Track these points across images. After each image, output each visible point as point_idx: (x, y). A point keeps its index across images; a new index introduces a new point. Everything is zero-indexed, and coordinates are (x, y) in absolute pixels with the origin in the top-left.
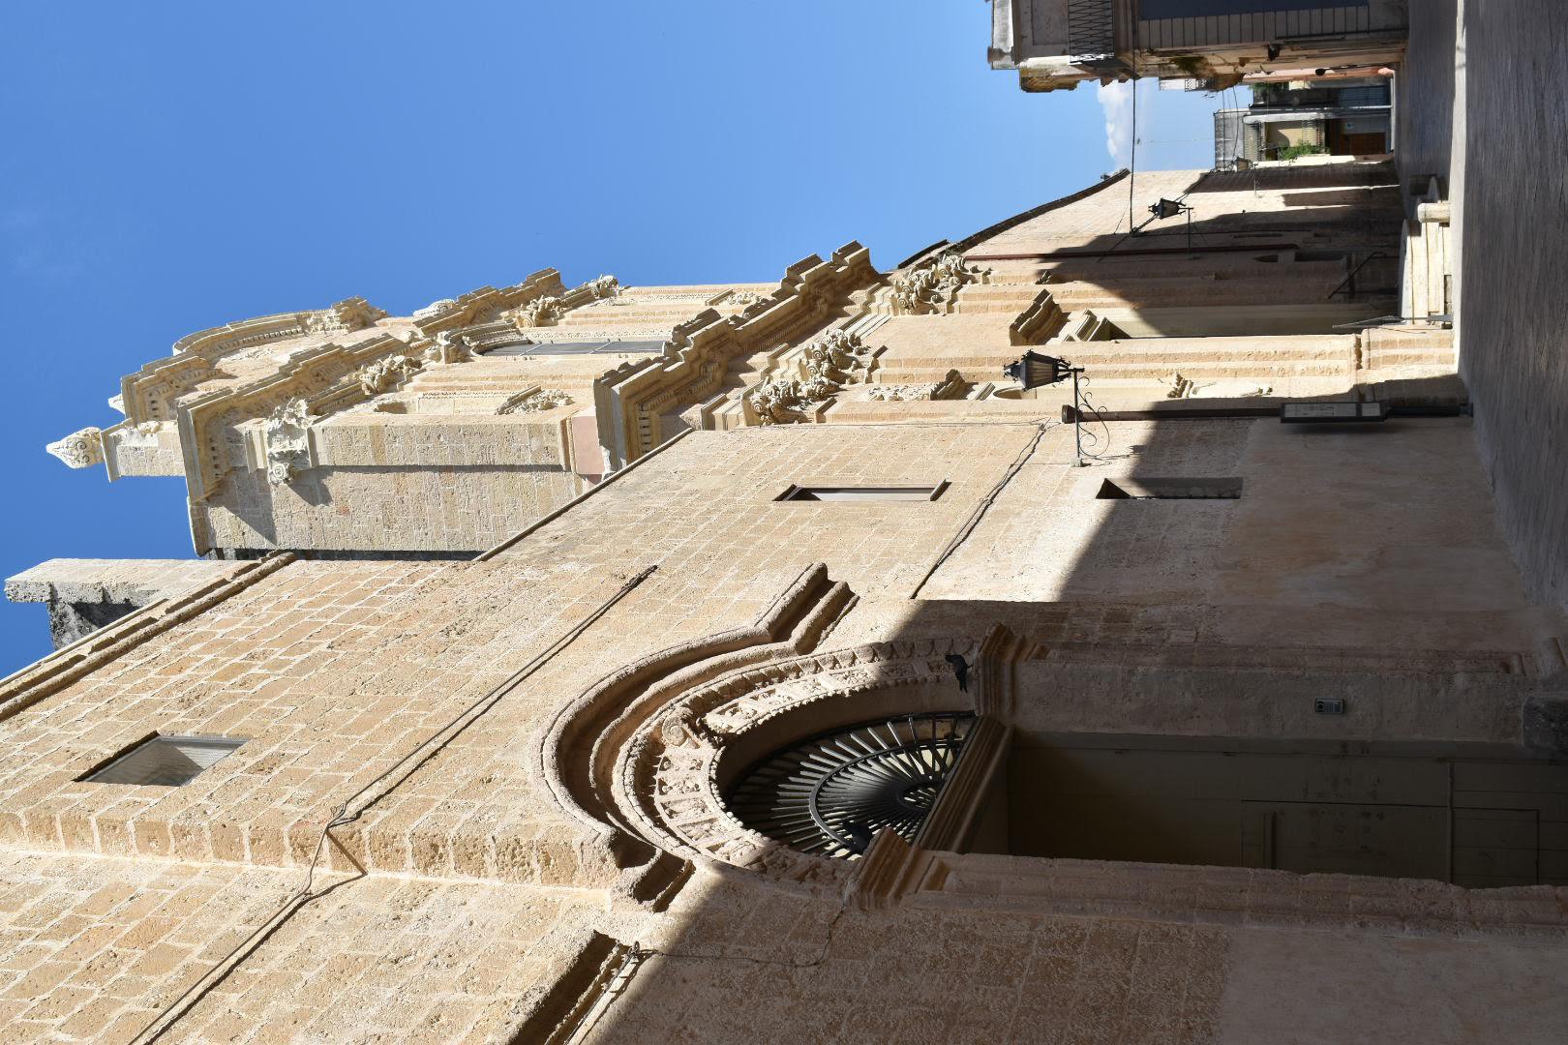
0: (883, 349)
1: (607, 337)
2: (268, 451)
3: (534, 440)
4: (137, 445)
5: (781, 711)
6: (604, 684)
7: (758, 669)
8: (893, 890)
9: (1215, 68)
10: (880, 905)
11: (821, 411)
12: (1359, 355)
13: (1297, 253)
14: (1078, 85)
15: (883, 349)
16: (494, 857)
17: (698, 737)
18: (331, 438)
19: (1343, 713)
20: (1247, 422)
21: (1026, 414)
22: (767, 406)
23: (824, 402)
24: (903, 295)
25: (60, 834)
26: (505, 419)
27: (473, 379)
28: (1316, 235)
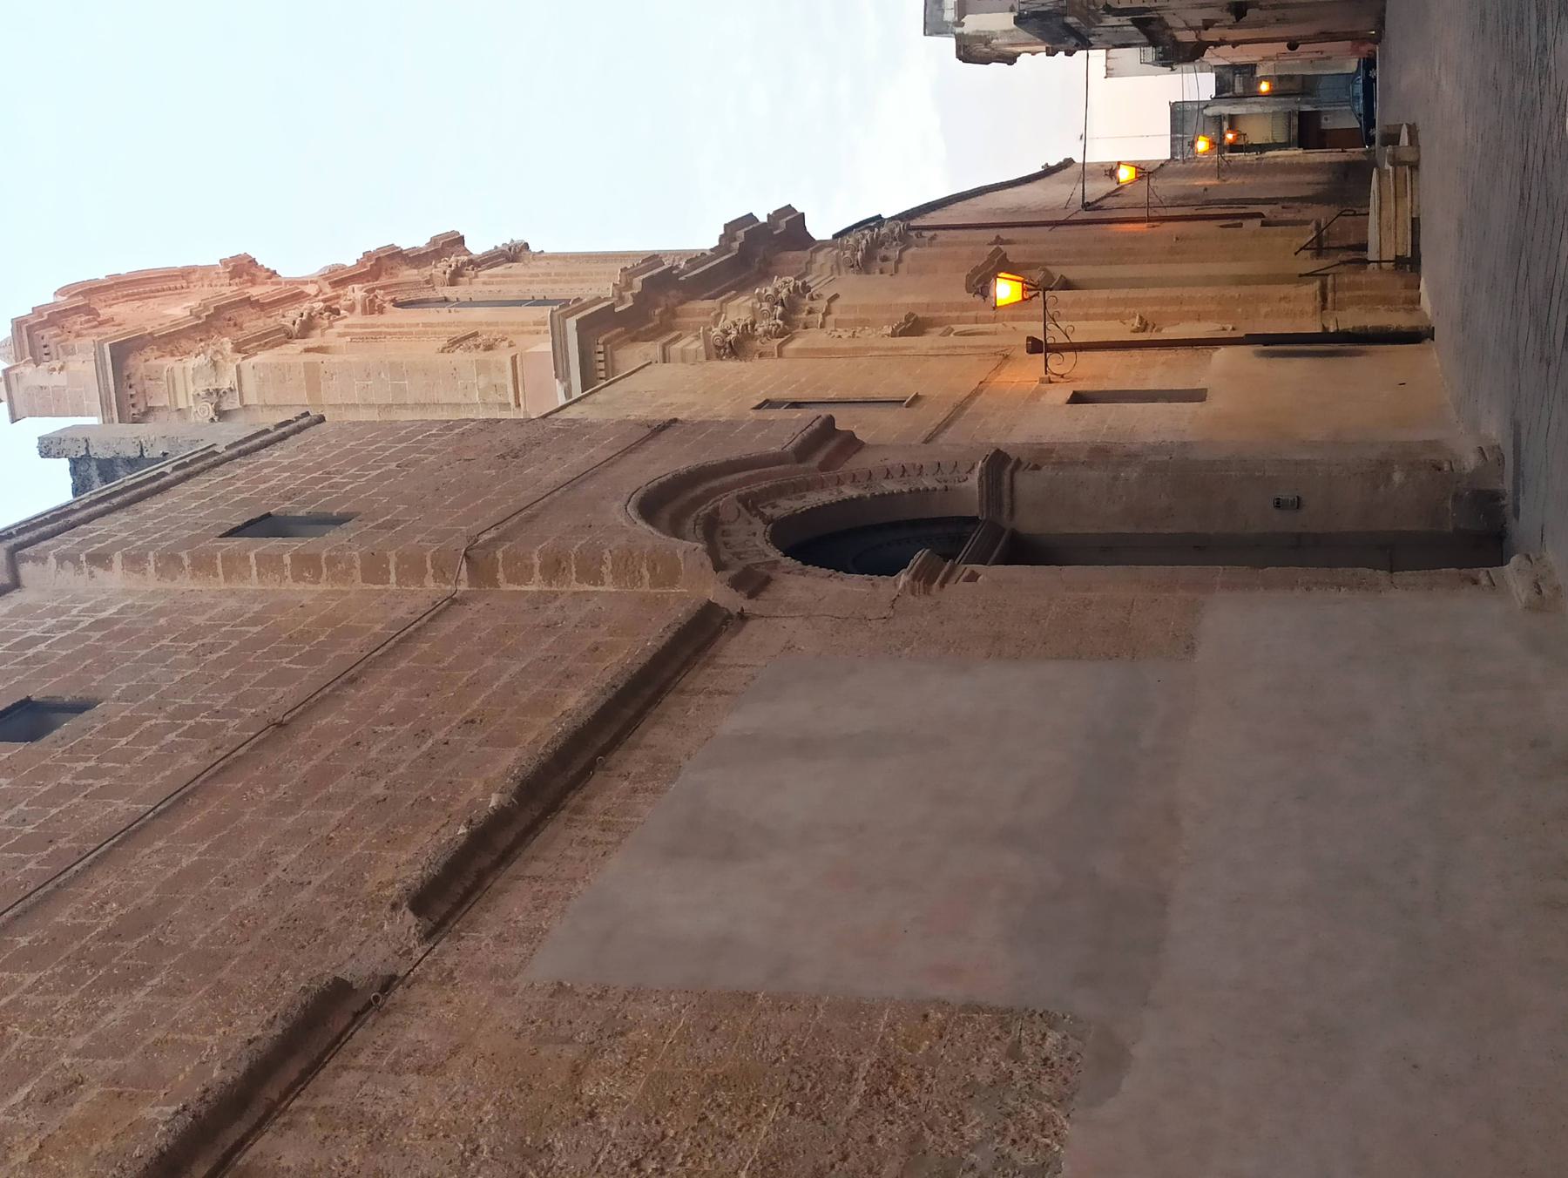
0: (836, 296)
1: (531, 294)
2: (191, 390)
3: (481, 377)
4: (43, 384)
5: (815, 506)
6: (664, 479)
7: (789, 479)
8: (940, 578)
9: (1176, 34)
10: (927, 592)
11: (780, 346)
12: (1324, 299)
13: (1262, 222)
14: (1018, 59)
15: (836, 296)
16: (610, 567)
17: (751, 515)
18: (262, 375)
19: (1298, 508)
20: (1210, 351)
21: (989, 346)
22: (728, 338)
23: (783, 339)
24: (848, 254)
25: (220, 570)
26: (447, 357)
27: (401, 326)
28: (1283, 208)
